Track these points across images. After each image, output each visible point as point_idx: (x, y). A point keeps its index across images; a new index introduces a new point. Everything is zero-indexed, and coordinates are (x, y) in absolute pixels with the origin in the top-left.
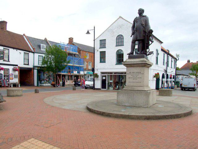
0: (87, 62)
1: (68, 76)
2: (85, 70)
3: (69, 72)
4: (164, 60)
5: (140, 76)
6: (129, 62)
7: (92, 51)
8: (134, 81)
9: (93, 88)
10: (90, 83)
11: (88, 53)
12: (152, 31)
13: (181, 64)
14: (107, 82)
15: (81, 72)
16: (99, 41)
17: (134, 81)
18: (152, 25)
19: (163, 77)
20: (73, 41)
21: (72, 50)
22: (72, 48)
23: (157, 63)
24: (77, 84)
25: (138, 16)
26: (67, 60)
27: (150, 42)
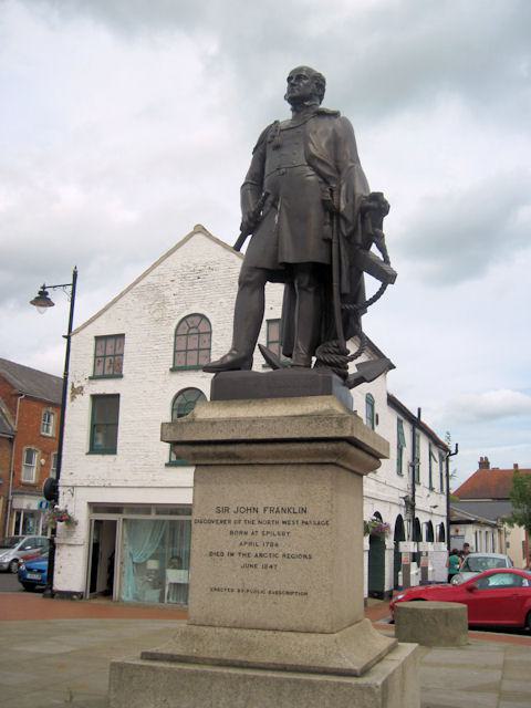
5: (299, 539)
6: (213, 423)
7: (55, 395)
8: (256, 578)
11: (50, 409)
13: (463, 469)
16: (93, 342)
17: (256, 578)
25: (285, 113)
27: (371, 284)
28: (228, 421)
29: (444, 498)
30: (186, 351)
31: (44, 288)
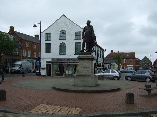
0: (27, 51)
6: (81, 57)
12: (96, 37)
13: (106, 54)
18: (96, 33)
25: (86, 25)
28: (82, 57)
29: (103, 59)
30: (64, 36)
31: (35, 24)
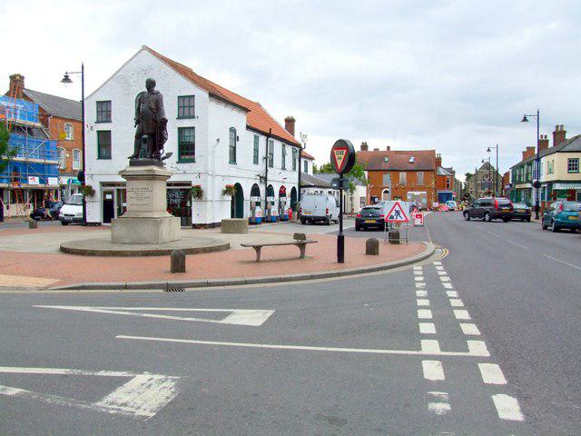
0: (69, 150)
1: (13, 191)
2: (63, 173)
3: (16, 180)
4: (256, 150)
9: (82, 222)
10: (76, 211)
14: (116, 207)
15: (49, 178)
19: (255, 191)
20: (23, 85)
21: (23, 116)
22: (20, 107)
23: (233, 159)
24: (37, 215)
26: (10, 147)
